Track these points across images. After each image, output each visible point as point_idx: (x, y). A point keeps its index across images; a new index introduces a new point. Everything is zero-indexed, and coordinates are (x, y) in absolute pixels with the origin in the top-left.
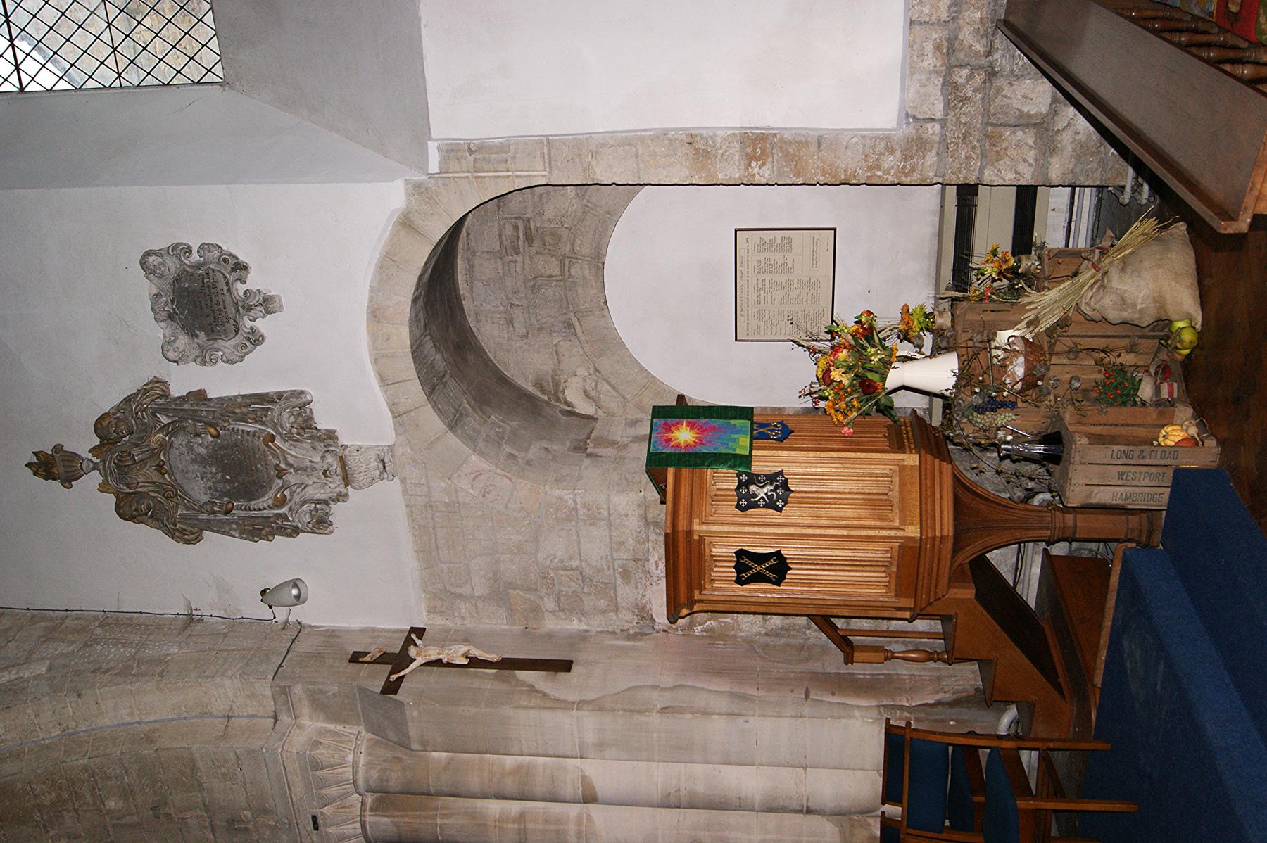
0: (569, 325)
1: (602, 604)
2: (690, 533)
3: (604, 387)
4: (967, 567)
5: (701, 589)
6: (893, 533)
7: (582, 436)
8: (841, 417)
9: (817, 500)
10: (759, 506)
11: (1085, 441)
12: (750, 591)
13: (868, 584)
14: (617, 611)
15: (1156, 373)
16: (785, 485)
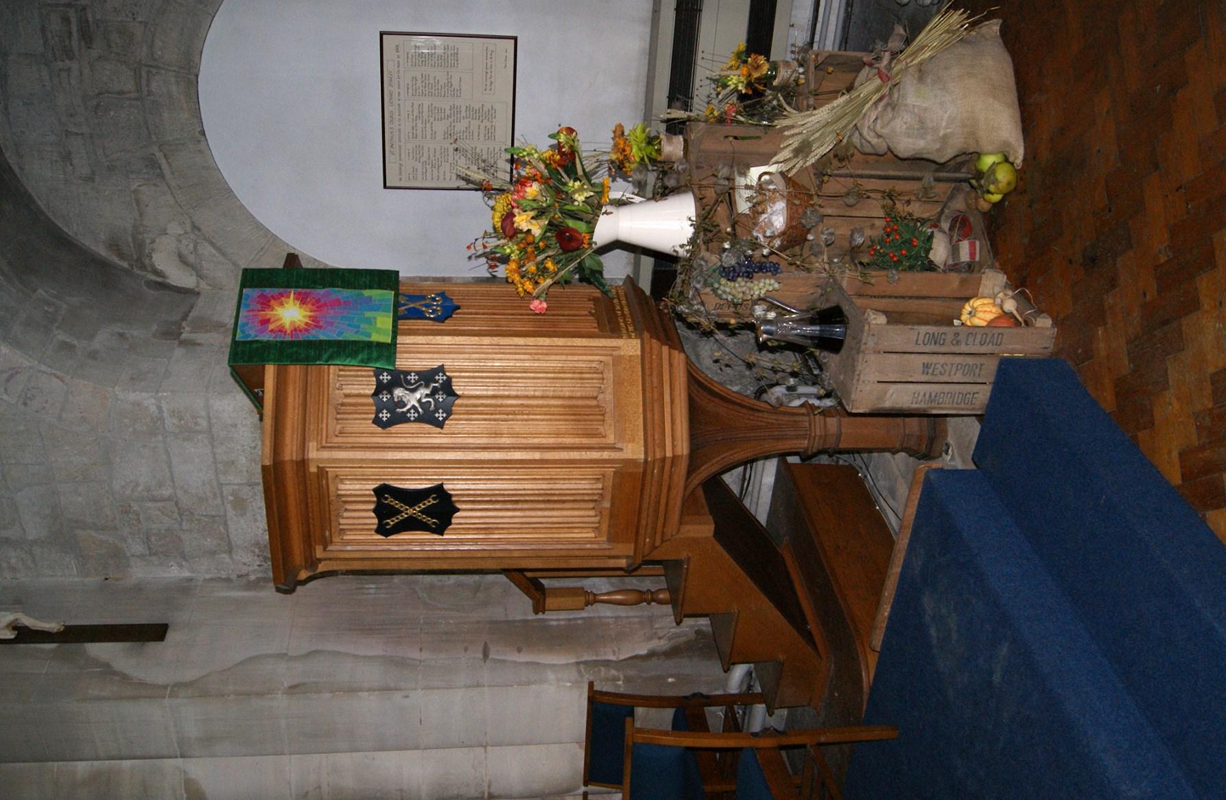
0: (152, 163)
1: (209, 543)
2: (303, 464)
3: (207, 250)
4: (700, 492)
5: (326, 543)
6: (606, 455)
7: (172, 313)
8: (529, 286)
9: (495, 409)
10: (408, 420)
11: (882, 319)
12: (398, 543)
13: (570, 527)
14: (230, 552)
15: (951, 228)
16: (447, 388)
